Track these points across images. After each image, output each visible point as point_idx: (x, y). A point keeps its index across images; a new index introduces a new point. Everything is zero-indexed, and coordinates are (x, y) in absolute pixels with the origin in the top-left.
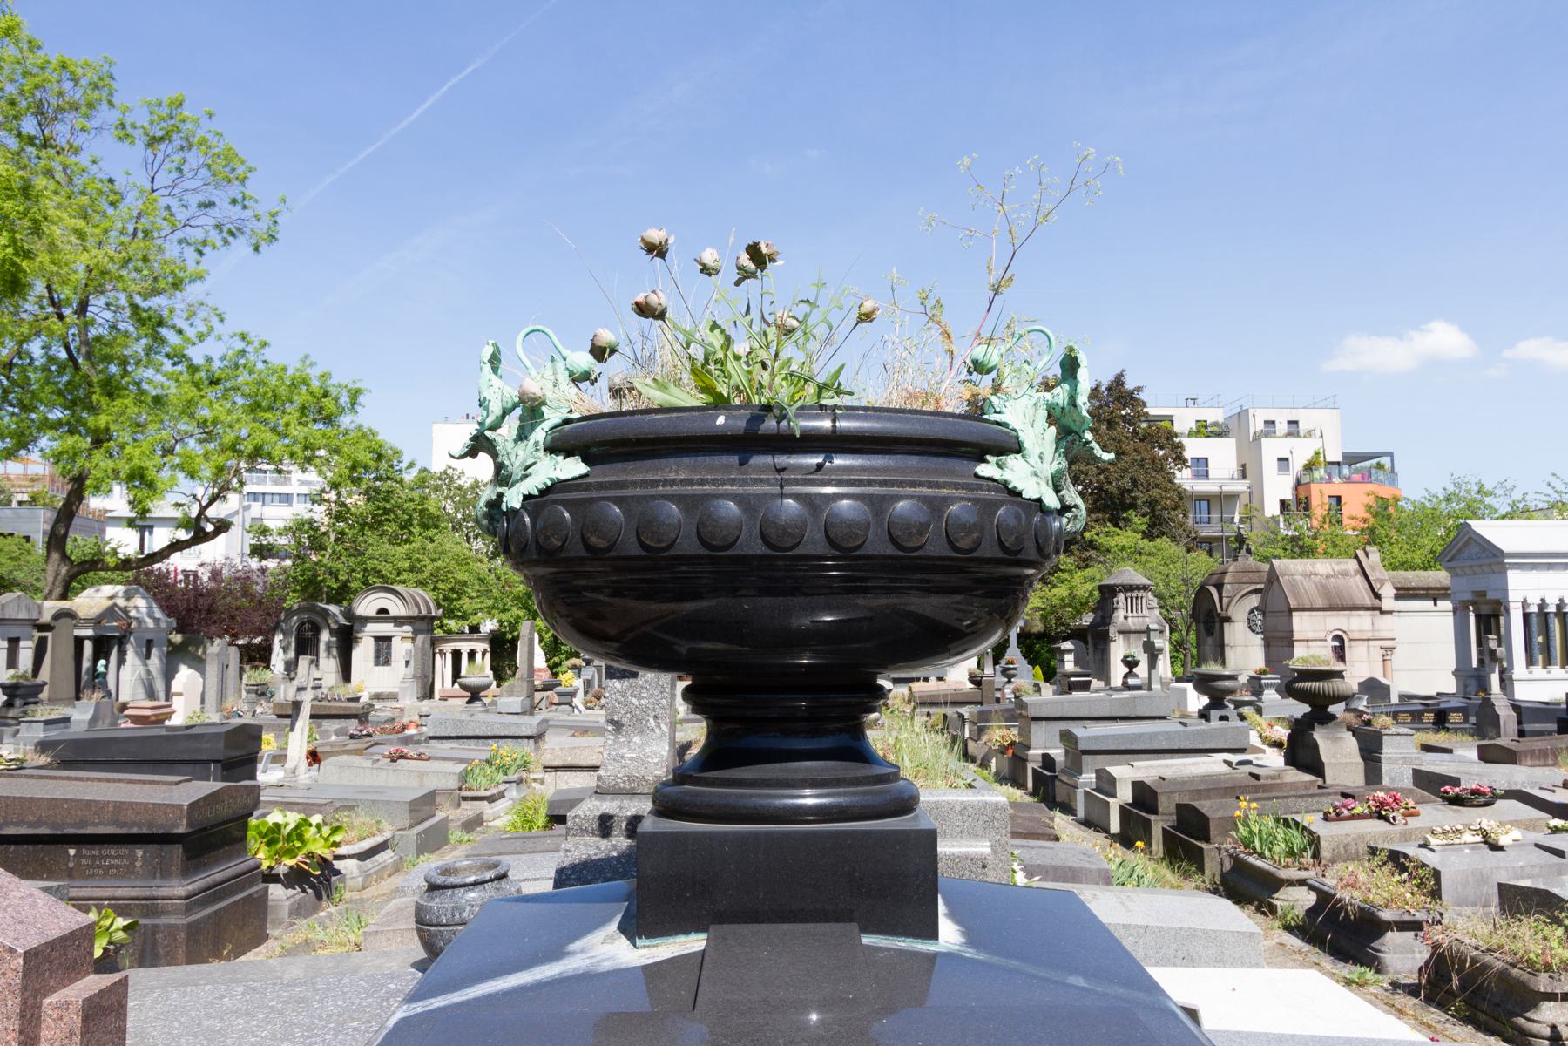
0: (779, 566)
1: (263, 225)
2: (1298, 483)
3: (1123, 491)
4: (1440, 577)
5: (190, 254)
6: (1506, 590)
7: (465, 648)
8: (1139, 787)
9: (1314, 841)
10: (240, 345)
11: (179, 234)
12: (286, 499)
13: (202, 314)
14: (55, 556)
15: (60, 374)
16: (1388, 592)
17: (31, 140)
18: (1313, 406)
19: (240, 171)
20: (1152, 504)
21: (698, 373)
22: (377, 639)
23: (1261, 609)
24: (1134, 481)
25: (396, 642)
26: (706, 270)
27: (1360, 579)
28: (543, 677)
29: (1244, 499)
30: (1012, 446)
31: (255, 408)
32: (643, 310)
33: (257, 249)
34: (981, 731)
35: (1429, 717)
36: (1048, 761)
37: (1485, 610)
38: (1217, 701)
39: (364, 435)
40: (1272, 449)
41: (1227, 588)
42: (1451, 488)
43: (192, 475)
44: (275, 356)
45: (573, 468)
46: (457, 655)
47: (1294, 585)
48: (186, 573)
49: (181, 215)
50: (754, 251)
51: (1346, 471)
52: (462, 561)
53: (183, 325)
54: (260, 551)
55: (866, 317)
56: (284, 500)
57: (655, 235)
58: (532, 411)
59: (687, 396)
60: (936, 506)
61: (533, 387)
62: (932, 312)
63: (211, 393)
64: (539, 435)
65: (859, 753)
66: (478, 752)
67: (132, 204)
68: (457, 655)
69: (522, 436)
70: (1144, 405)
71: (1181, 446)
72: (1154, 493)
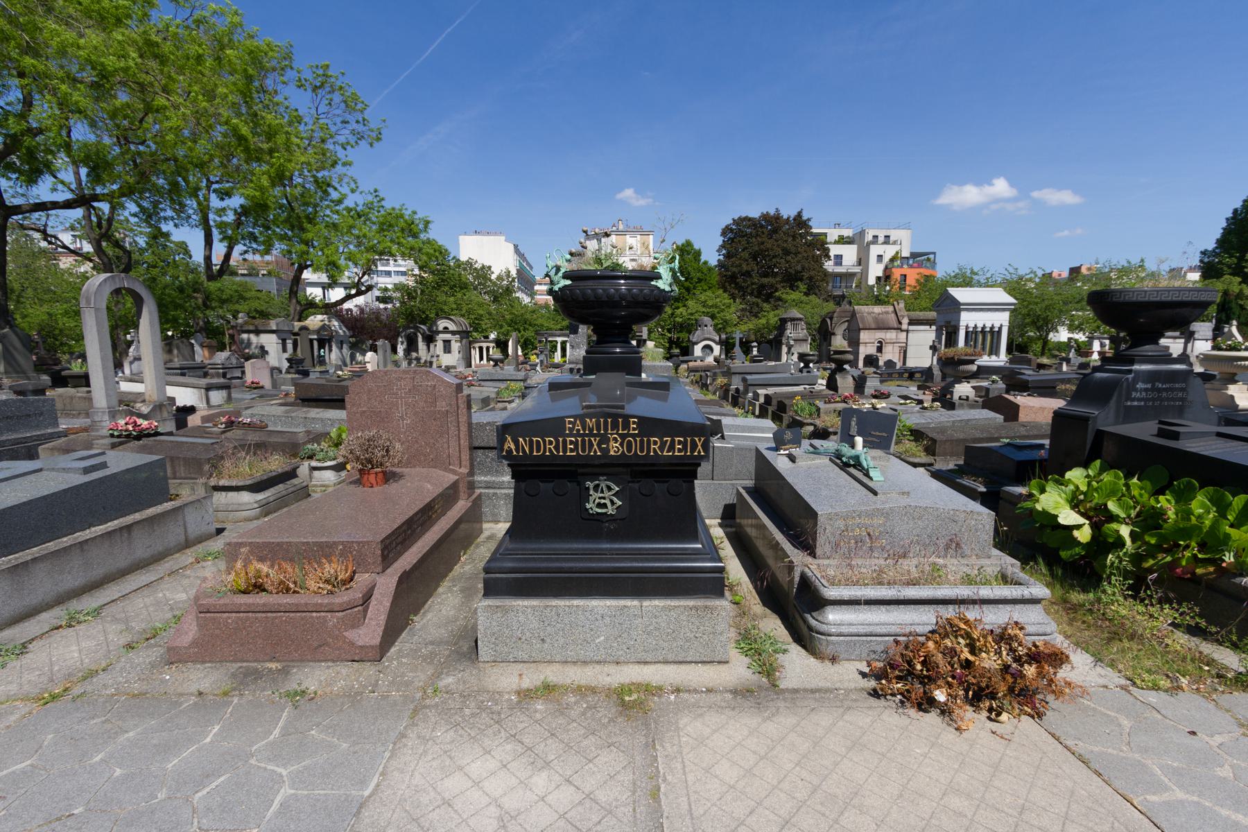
0: (613, 303)
2: (886, 268)
3: (797, 272)
4: (932, 315)
5: (339, 148)
7: (484, 345)
8: (767, 396)
9: (818, 410)
13: (346, 180)
16: (905, 321)
18: (898, 228)
20: (811, 278)
23: (848, 328)
28: (521, 359)
30: (659, 277)
34: (714, 380)
36: (737, 390)
37: (950, 330)
39: (429, 242)
40: (875, 250)
41: (835, 319)
43: (356, 265)
45: (568, 282)
46: (481, 349)
47: (863, 318)
52: (480, 305)
53: (337, 186)
56: (396, 273)
60: (641, 291)
63: (359, 222)
64: (560, 274)
66: (502, 385)
68: (481, 349)
71: (828, 250)
72: (812, 273)
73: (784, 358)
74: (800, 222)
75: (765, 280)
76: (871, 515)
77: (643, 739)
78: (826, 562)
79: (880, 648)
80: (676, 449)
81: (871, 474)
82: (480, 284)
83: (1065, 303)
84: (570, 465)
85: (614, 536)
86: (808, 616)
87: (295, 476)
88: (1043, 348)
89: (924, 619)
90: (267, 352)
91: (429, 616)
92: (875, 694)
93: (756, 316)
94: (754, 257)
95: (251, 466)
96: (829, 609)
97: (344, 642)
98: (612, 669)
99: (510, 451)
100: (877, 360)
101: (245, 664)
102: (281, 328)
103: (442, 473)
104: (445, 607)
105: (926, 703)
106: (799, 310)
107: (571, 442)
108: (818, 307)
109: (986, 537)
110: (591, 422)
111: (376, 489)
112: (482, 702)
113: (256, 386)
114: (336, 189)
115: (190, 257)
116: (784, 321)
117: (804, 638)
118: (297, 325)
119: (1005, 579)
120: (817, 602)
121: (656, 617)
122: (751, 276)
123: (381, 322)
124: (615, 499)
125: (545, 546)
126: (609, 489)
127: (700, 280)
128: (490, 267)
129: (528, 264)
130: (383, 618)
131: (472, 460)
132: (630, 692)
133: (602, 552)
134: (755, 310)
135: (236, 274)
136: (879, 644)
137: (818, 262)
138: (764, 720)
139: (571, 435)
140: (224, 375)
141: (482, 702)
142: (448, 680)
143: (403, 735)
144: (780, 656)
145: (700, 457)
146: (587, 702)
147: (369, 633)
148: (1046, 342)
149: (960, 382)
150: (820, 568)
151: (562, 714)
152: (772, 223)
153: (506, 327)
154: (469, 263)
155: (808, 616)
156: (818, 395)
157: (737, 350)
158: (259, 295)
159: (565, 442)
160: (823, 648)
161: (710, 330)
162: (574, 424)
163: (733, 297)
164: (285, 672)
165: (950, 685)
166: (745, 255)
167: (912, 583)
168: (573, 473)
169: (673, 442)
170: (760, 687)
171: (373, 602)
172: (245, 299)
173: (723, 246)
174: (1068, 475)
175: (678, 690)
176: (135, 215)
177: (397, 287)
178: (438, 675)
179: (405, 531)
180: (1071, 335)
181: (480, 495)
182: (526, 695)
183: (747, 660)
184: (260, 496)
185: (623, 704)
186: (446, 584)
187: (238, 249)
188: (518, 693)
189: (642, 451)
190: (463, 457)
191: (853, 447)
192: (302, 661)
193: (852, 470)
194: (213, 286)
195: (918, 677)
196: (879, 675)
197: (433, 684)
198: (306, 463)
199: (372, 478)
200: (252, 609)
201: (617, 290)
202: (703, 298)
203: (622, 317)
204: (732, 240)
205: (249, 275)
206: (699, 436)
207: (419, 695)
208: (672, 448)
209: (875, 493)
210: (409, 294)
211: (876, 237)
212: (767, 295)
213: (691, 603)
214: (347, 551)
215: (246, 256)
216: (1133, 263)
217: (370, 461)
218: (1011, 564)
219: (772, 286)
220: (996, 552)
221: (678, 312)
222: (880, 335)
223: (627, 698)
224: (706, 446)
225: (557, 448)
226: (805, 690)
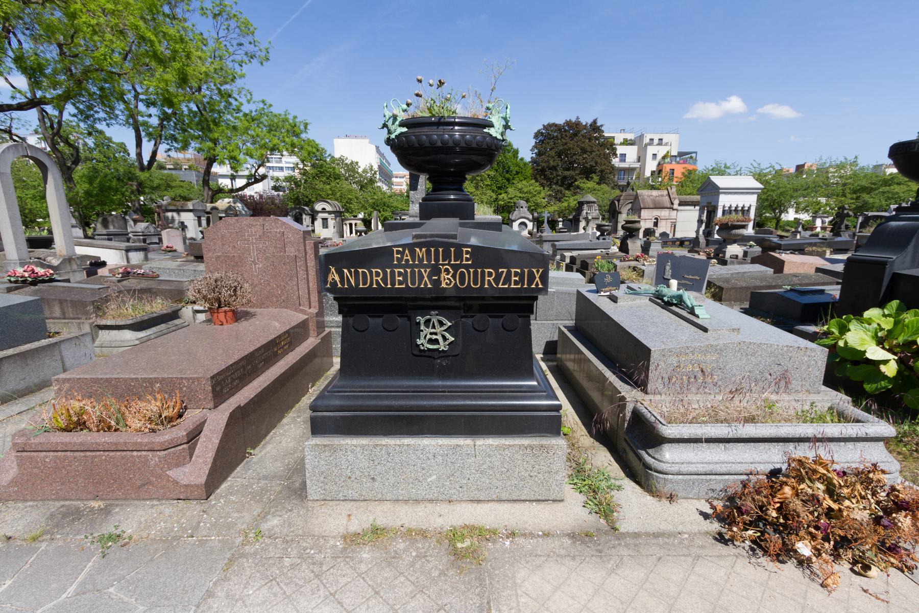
0: (447, 149)
1: (263, 54)
2: (659, 164)
3: (592, 166)
4: (697, 198)
5: (236, 65)
6: (718, 202)
7: (353, 222)
8: (572, 258)
9: (615, 266)
10: (261, 105)
11: (231, 58)
12: (281, 169)
13: (244, 92)
14: (206, 188)
15: (195, 117)
16: (676, 202)
17: (168, 16)
18: (669, 133)
19: (252, 29)
21: (429, 109)
22: (323, 219)
24: (596, 163)
25: (329, 220)
26: (431, 85)
27: (667, 198)
29: (638, 170)
30: (491, 125)
31: (270, 131)
32: (417, 95)
33: (262, 64)
35: (678, 243)
37: (710, 209)
38: (602, 234)
40: (651, 150)
42: (714, 165)
43: (252, 157)
44: (276, 110)
45: (405, 130)
46: (351, 225)
47: (643, 200)
48: (250, 196)
49: (231, 50)
50: (440, 81)
51: (678, 159)
52: (350, 191)
53: (237, 97)
54: (275, 188)
55: (464, 97)
56: (285, 165)
57: (419, 78)
58: (395, 118)
59: (427, 114)
61: (395, 112)
62: (478, 96)
63: (254, 125)
64: (397, 123)
65: (462, 190)
67: (212, 45)
68: (351, 225)
69: (393, 124)
70: (603, 132)
72: (603, 167)
73: (582, 231)
74: (595, 127)
75: (567, 173)
76: (705, 351)
77: (476, 600)
78: (658, 397)
79: (719, 487)
80: (512, 281)
81: (697, 311)
82: (350, 176)
83: (796, 190)
84: (401, 298)
85: (444, 373)
86: (643, 453)
87: (178, 317)
88: (777, 225)
89: (773, 457)
90: (186, 227)
91: (269, 448)
92: (721, 538)
93: (560, 201)
94: (559, 155)
95: (134, 308)
96: (666, 447)
97: (168, 481)
98: (443, 508)
99: (334, 284)
100: (654, 232)
101: (67, 503)
102: (196, 208)
103: (292, 313)
104: (290, 433)
105: (786, 553)
106: (593, 194)
107: (400, 274)
108: (608, 193)
109: (817, 373)
110: (421, 252)
111: (225, 327)
112: (305, 549)
113: (170, 250)
114: (236, 100)
115: (129, 155)
116: (581, 204)
117: (640, 474)
118: (209, 206)
119: (842, 417)
120: (655, 440)
121: (489, 456)
122: (556, 170)
123: (275, 205)
124: (447, 335)
125: (374, 383)
126: (441, 324)
127: (517, 173)
128: (357, 163)
129: (387, 161)
130: (211, 455)
131: (320, 302)
132: (463, 538)
133: (434, 390)
134: (559, 196)
135: (165, 168)
136: (718, 483)
137: (607, 158)
138: (609, 575)
139: (399, 266)
140: (144, 241)
141: (305, 549)
142: (274, 522)
143: (210, 594)
144: (614, 493)
145: (539, 290)
146: (417, 549)
147: (195, 471)
148: (778, 220)
149: (731, 244)
150: (654, 404)
151: (389, 564)
152: (574, 128)
153: (370, 209)
154: (341, 160)
155: (643, 453)
156: (614, 256)
157: (546, 225)
158: (182, 184)
159: (393, 273)
160: (660, 486)
161: (525, 211)
162: (402, 253)
163: (542, 185)
164: (106, 512)
165: (813, 537)
166: (553, 153)
167: (751, 420)
168: (405, 306)
169: (509, 273)
170: (598, 530)
171: (202, 438)
172: (171, 187)
173: (535, 147)
174: (867, 314)
175: (513, 534)
176: (74, 115)
177: (289, 179)
178: (263, 516)
179: (243, 366)
180: (798, 216)
181: (330, 332)
182: (353, 539)
183: (582, 498)
184: (142, 334)
185: (457, 554)
186: (291, 414)
187: (163, 147)
188: (344, 537)
189: (476, 283)
190: (312, 299)
191: (668, 286)
192: (126, 499)
193: (674, 308)
194: (143, 176)
195: (771, 524)
196: (726, 519)
197: (257, 526)
198: (190, 307)
199: (222, 316)
200: (70, 448)
201: (451, 136)
202: (520, 186)
203: (456, 164)
204: (542, 141)
205: (175, 169)
206: (538, 268)
207: (238, 541)
208: (508, 280)
209: (705, 330)
210: (296, 183)
211: (652, 140)
212: (568, 184)
213: (525, 441)
214: (169, 386)
215: (170, 153)
216: (849, 159)
217: (218, 300)
218: (841, 400)
219: (572, 177)
220: (824, 388)
221: (500, 197)
222: (656, 213)
223: (459, 545)
224: (544, 278)
225: (384, 280)
226: (647, 534)
